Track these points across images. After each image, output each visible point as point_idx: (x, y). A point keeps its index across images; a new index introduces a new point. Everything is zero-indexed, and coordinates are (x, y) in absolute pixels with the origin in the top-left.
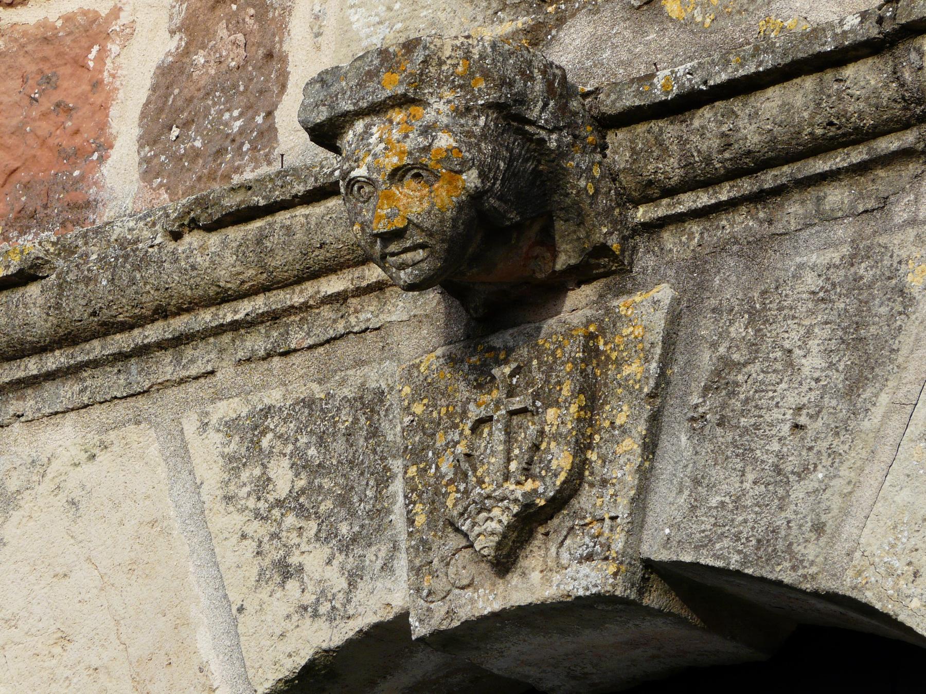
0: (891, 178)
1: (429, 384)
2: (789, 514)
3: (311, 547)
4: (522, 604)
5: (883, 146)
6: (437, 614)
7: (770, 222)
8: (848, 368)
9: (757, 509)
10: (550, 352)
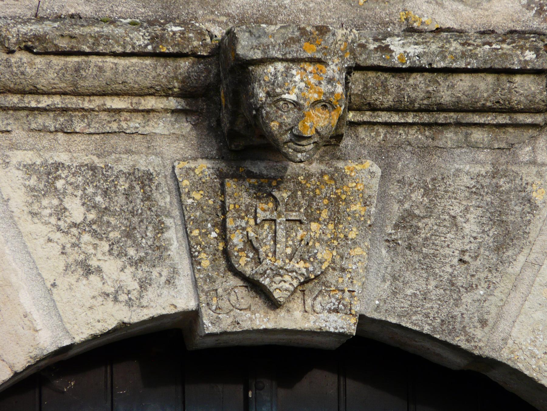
0: (516, 134)
1: (204, 183)
2: (462, 309)
3: (106, 258)
4: (289, 328)
5: (521, 119)
6: (224, 323)
7: (433, 139)
8: (495, 237)
9: (439, 302)
10: (310, 189)
